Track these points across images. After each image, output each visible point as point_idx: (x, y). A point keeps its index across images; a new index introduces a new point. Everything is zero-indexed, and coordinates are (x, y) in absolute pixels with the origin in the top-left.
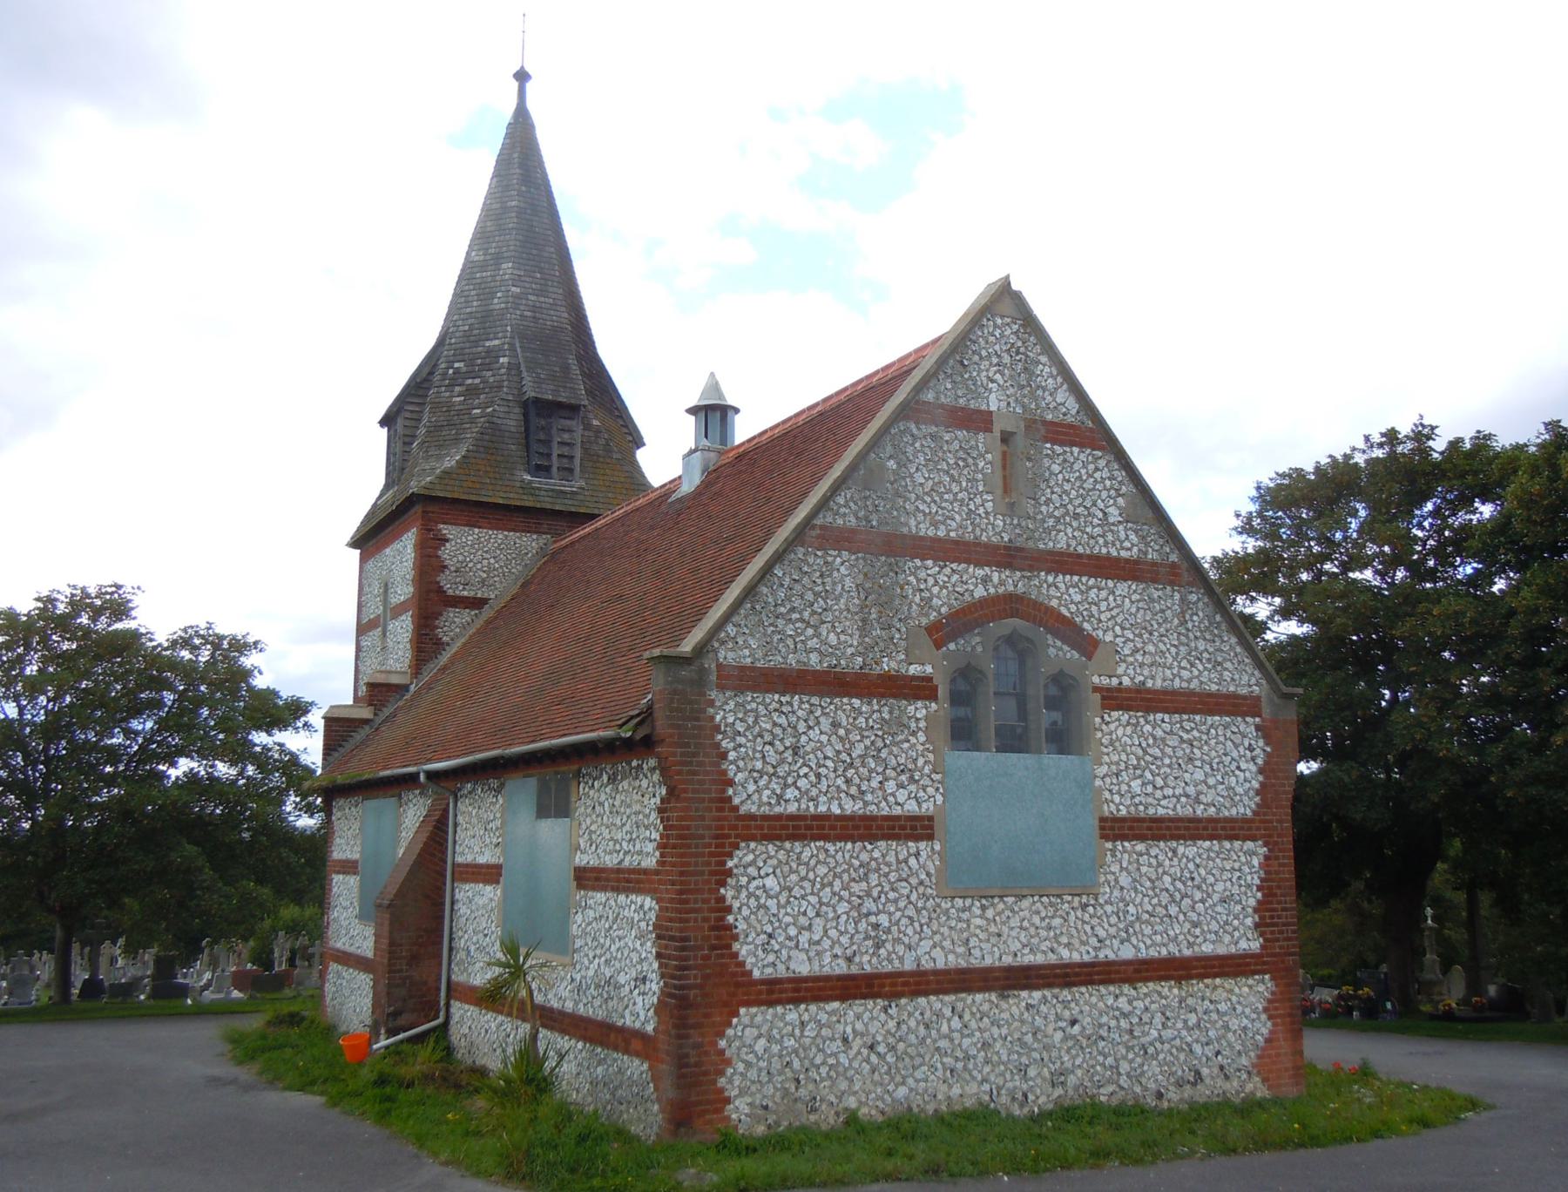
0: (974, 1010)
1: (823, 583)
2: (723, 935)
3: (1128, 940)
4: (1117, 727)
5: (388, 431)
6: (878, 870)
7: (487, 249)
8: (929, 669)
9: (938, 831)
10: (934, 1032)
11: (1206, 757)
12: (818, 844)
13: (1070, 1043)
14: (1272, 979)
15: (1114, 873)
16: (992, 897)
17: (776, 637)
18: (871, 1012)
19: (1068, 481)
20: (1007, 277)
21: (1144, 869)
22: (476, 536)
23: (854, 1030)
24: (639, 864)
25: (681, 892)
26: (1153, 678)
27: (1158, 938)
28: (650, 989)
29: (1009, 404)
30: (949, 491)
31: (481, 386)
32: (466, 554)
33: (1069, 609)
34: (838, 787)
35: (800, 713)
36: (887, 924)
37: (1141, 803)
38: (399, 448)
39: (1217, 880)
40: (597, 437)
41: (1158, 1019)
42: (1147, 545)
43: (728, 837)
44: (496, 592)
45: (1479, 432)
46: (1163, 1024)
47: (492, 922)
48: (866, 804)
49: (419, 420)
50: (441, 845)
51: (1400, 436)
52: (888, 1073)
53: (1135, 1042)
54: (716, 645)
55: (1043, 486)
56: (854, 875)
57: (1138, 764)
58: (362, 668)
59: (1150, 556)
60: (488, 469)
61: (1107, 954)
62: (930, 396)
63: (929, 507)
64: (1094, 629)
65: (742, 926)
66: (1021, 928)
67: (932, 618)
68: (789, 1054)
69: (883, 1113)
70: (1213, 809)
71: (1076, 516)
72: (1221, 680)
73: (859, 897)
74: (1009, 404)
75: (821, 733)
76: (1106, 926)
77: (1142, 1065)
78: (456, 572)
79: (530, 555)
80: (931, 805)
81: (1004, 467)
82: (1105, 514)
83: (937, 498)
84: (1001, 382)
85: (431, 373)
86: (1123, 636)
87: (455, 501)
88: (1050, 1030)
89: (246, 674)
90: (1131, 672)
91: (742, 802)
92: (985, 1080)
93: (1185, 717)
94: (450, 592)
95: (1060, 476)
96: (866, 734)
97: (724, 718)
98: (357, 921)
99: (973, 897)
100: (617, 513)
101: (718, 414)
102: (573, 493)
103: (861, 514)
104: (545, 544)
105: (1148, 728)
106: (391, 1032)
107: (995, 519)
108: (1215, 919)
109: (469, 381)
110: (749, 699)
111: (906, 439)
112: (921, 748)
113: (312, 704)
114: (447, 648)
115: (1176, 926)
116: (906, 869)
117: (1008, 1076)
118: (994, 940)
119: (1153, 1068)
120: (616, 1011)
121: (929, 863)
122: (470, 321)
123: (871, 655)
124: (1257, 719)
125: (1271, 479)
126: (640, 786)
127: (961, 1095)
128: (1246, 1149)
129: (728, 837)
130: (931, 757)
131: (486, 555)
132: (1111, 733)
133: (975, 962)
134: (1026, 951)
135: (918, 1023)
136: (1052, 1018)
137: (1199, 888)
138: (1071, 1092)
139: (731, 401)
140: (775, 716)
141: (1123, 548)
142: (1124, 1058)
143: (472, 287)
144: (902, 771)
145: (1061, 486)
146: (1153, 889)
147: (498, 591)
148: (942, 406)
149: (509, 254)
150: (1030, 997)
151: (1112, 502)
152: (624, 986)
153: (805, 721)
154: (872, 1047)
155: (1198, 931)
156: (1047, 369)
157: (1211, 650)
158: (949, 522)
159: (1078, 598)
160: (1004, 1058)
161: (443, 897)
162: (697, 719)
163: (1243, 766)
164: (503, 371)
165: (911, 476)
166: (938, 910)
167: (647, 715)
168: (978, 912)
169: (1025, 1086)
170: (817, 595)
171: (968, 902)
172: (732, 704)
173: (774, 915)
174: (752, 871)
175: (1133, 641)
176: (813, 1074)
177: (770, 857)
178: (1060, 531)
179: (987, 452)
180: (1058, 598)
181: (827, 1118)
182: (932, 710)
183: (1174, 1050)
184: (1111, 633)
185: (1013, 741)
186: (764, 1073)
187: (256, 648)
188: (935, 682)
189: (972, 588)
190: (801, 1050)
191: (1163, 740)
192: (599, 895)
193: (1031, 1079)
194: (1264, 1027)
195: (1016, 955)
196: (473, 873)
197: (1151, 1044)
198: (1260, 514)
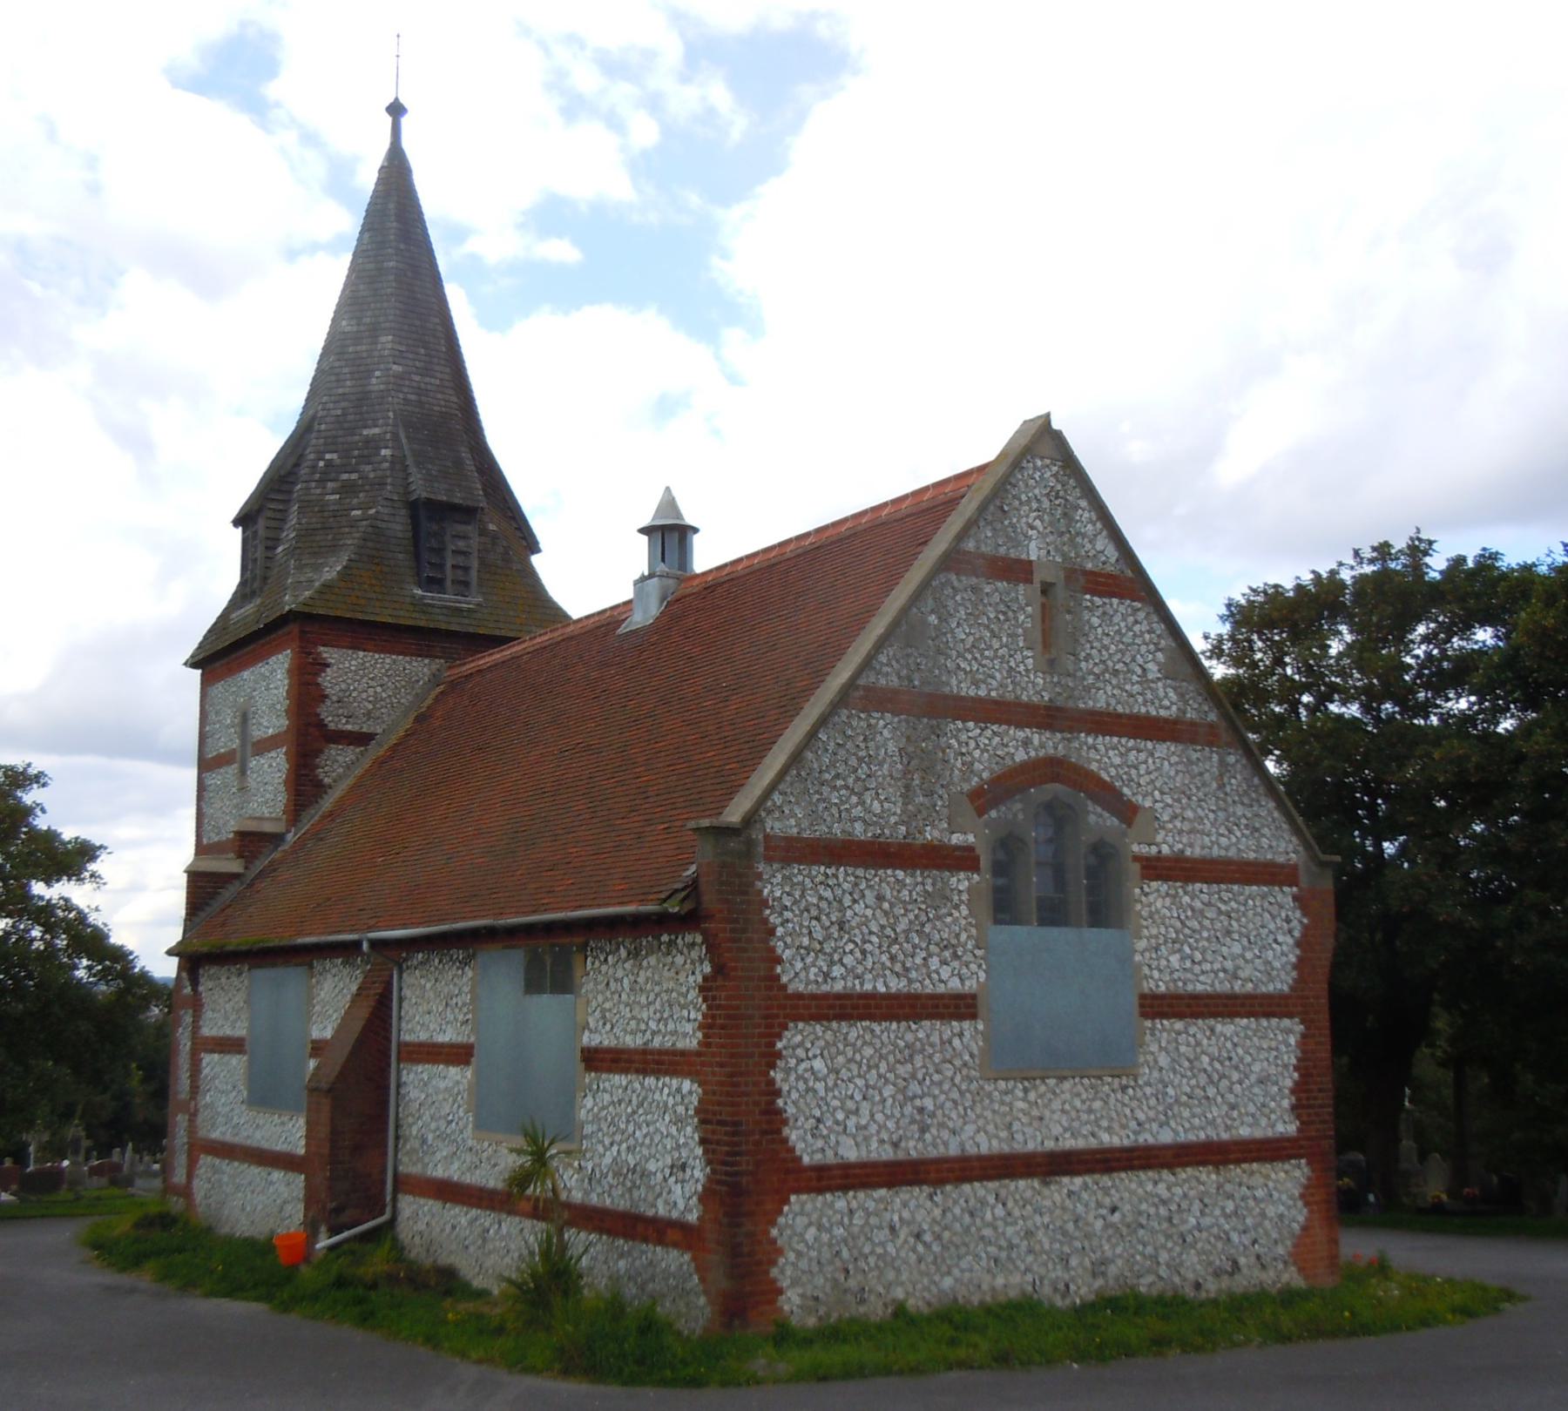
0: (1018, 1197)
2: (774, 1119)
3: (1168, 1124)
5: (244, 532)
6: (922, 1051)
8: (971, 838)
9: (982, 1010)
10: (978, 1221)
11: (1244, 930)
12: (864, 1024)
13: (1110, 1231)
14: (1309, 1164)
15: (1152, 1053)
16: (1034, 1079)
17: (821, 806)
18: (917, 1199)
19: (1108, 635)
20: (1048, 415)
21: (1183, 1049)
23: (901, 1219)
24: (673, 1045)
25: (732, 1075)
26: (1191, 845)
27: (1196, 1121)
28: (692, 1176)
29: (1049, 552)
30: (989, 647)
31: (360, 482)
33: (1108, 773)
34: (883, 964)
35: (846, 886)
37: (1180, 979)
38: (260, 553)
39: (1254, 1060)
41: (1197, 1206)
42: (1186, 703)
43: (777, 1016)
44: (384, 726)
45: (1484, 549)
47: (459, 1107)
48: (910, 981)
49: (283, 520)
51: (1393, 551)
52: (935, 1262)
53: (1174, 1230)
54: (763, 814)
55: (1083, 640)
56: (899, 1056)
57: (1177, 937)
58: (208, 811)
59: (1189, 715)
60: (374, 582)
61: (1146, 1138)
62: (970, 545)
63: (970, 665)
64: (1134, 794)
65: (791, 1110)
66: (1063, 1111)
68: (838, 1243)
71: (1116, 673)
72: (1259, 847)
73: (905, 1080)
74: (1049, 552)
75: (866, 907)
76: (1145, 1108)
77: (1181, 1254)
80: (974, 981)
81: (1043, 621)
82: (1144, 670)
83: (978, 655)
84: (1041, 529)
85: (297, 465)
86: (1162, 801)
87: (338, 619)
88: (1091, 1218)
89: (27, 812)
90: (1170, 839)
91: (790, 981)
92: (1028, 1270)
93: (1223, 886)
94: (332, 726)
95: (1100, 630)
96: (910, 907)
97: (772, 891)
98: (244, 1107)
99: (1015, 1079)
100: (539, 640)
101: (676, 535)
102: (469, 610)
105: (1186, 899)
106: (334, 1231)
107: (1036, 677)
108: (1253, 1101)
109: (345, 476)
110: (796, 871)
111: (949, 591)
112: (964, 922)
113: (101, 847)
115: (1214, 1109)
116: (950, 1050)
117: (1050, 1266)
118: (1036, 1124)
119: (1191, 1258)
120: (645, 1200)
123: (914, 824)
124: (1295, 889)
125: (1244, 595)
126: (673, 963)
127: (1005, 1286)
128: (1300, 1337)
129: (777, 1016)
130: (974, 931)
131: (372, 683)
132: (1150, 905)
133: (1018, 1147)
134: (1067, 1135)
135: (962, 1210)
136: (1093, 1205)
137: (1237, 1068)
138: (1111, 1282)
139: (689, 519)
140: (821, 889)
141: (1162, 707)
142: (1164, 1247)
143: (343, 363)
144: (945, 947)
146: (1191, 1069)
147: (389, 724)
148: (983, 556)
149: (388, 325)
150: (1072, 1183)
151: (1151, 656)
152: (655, 1174)
153: (851, 894)
154: (918, 1236)
155: (1235, 1114)
156: (1086, 515)
157: (1249, 815)
158: (989, 680)
159: (1117, 761)
160: (1047, 1247)
161: (387, 1078)
162: (745, 893)
163: (1280, 939)
165: (952, 631)
166: (982, 1093)
167: (694, 886)
168: (1021, 1094)
169: (1066, 1277)
170: (861, 760)
171: (1010, 1085)
172: (779, 876)
173: (822, 1098)
174: (800, 1052)
175: (1171, 806)
176: (862, 1264)
177: (818, 1038)
178: (1099, 689)
179: (1027, 605)
180: (1097, 761)
181: (876, 1310)
182: (974, 882)
183: (1212, 1240)
184: (1150, 798)
185: (1053, 914)
186: (814, 1263)
187: (38, 782)
188: (978, 851)
189: (1012, 751)
190: (850, 1240)
191: (1202, 912)
192: (617, 1077)
193: (1073, 1269)
194: (1300, 1215)
195: (1057, 1139)
196: (428, 1053)
197: (1190, 1232)
198: (1232, 638)
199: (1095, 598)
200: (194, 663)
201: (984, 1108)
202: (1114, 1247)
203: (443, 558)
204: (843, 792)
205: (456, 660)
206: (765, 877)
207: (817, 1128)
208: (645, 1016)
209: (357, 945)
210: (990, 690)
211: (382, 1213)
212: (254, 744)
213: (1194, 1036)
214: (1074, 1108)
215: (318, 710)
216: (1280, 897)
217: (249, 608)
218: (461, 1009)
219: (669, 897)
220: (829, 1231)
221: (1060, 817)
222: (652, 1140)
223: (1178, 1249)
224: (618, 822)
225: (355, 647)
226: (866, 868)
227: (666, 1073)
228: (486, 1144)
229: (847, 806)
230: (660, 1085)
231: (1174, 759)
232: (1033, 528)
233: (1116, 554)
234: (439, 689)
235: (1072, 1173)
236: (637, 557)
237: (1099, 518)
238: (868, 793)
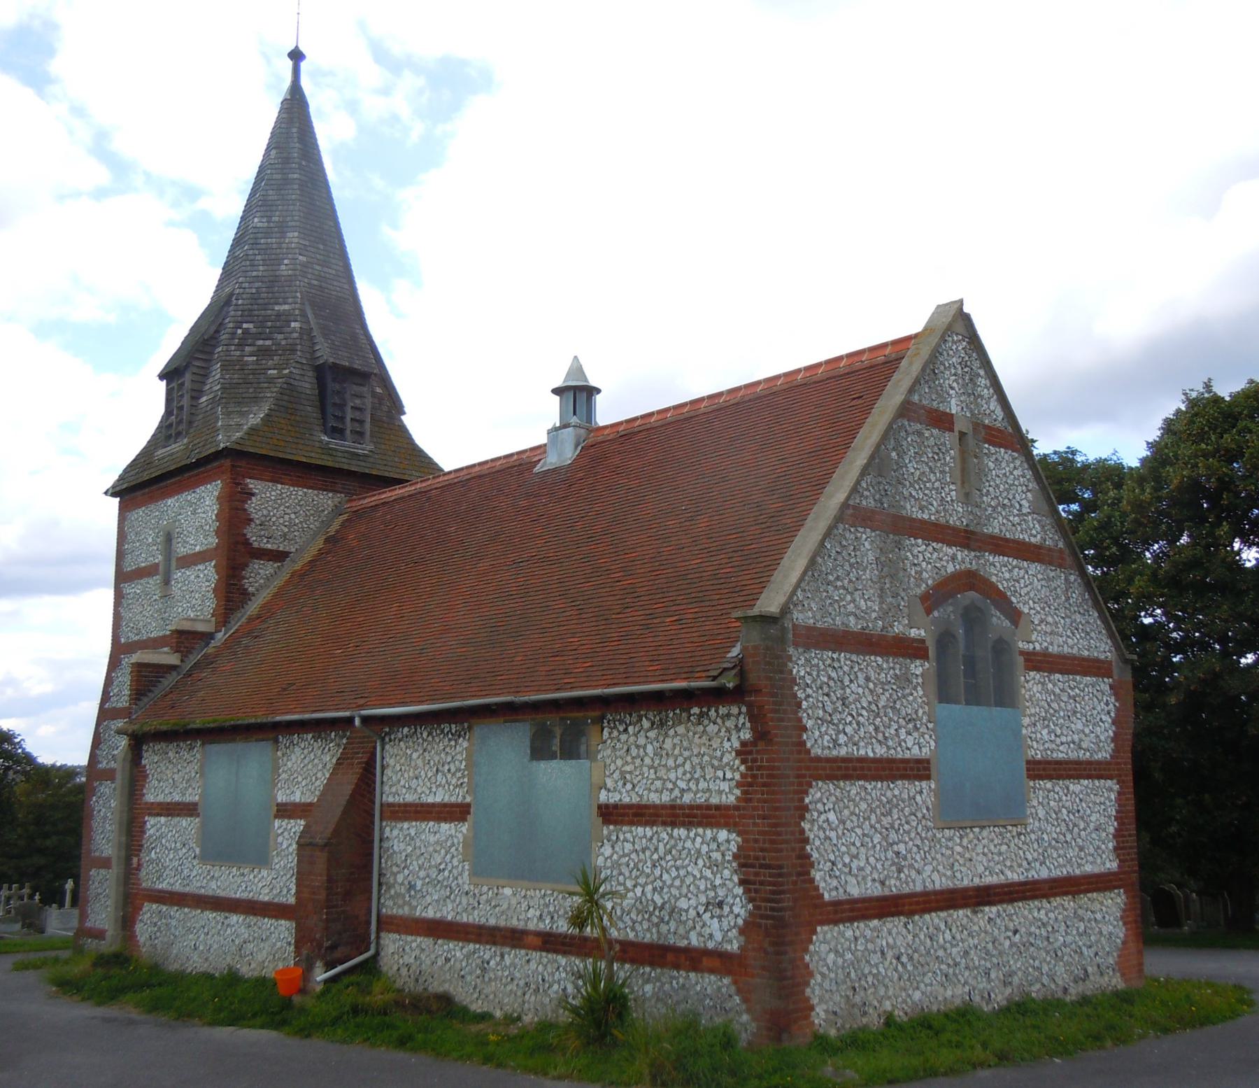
0: (959, 924)
1: (856, 556)
3: (1045, 863)
4: (1032, 685)
5: (168, 385)
7: (271, 217)
8: (923, 634)
9: (933, 773)
12: (860, 783)
15: (1034, 807)
16: (966, 828)
20: (961, 302)
21: (1052, 803)
22: (279, 492)
23: (887, 943)
26: (1052, 644)
31: (274, 348)
32: (270, 508)
33: (1003, 584)
36: (904, 852)
39: (1092, 812)
40: (380, 404)
41: (1063, 927)
45: (1069, 448)
46: (1066, 931)
47: (453, 857)
48: (888, 748)
49: (206, 376)
50: (370, 786)
52: (909, 980)
56: (883, 810)
59: (1047, 543)
60: (290, 428)
61: (1033, 875)
63: (918, 494)
65: (815, 855)
66: (984, 854)
67: (923, 589)
69: (906, 1014)
70: (1088, 754)
74: (962, 408)
75: (859, 686)
76: (1032, 851)
77: (1055, 966)
78: (261, 525)
79: (326, 512)
82: (1021, 505)
85: (217, 331)
86: (1034, 609)
90: (1039, 638)
93: (1071, 677)
94: (256, 545)
96: (886, 687)
99: (954, 828)
103: (877, 497)
104: (340, 503)
105: (1050, 686)
106: (329, 966)
109: (260, 342)
110: (813, 655)
111: (903, 434)
112: (920, 700)
114: (253, 598)
115: (1071, 850)
119: (1060, 969)
121: (928, 800)
122: (257, 285)
124: (1111, 680)
127: (953, 996)
131: (288, 511)
133: (959, 884)
136: (1003, 928)
137: (1082, 818)
139: (593, 382)
140: (830, 670)
141: (1031, 535)
144: (910, 720)
145: (994, 481)
146: (1057, 819)
147: (303, 546)
148: (923, 407)
149: (293, 224)
154: (898, 959)
156: (983, 382)
157: (1083, 622)
159: (1007, 575)
162: (782, 672)
163: (1104, 718)
164: (295, 335)
167: (740, 666)
170: (851, 565)
173: (835, 845)
174: (820, 806)
178: (995, 519)
181: (873, 1020)
182: (925, 668)
189: (945, 564)
193: (993, 981)
194: (1121, 932)
195: (981, 877)
199: (991, 447)
200: (114, 492)
201: (936, 852)
202: (1016, 962)
203: (343, 412)
204: (841, 591)
205: (353, 494)
206: (794, 659)
207: (832, 870)
208: (672, 776)
209: (350, 720)
210: (930, 515)
211: (367, 950)
212: (178, 559)
213: (1058, 793)
214: (990, 850)
215: (245, 531)
216: (1102, 685)
217: (176, 447)
218: (454, 774)
219: (720, 674)
220: (842, 956)
221: (973, 618)
222: (682, 881)
223: (1053, 962)
224: (614, 616)
225: (275, 480)
226: (858, 655)
227: (700, 824)
228: (485, 889)
229: (844, 603)
230: (692, 835)
231: (1040, 576)
232: (952, 388)
233: (1002, 413)
234: (342, 518)
235: (991, 903)
236: (551, 411)
237: (992, 385)
238: (858, 593)
